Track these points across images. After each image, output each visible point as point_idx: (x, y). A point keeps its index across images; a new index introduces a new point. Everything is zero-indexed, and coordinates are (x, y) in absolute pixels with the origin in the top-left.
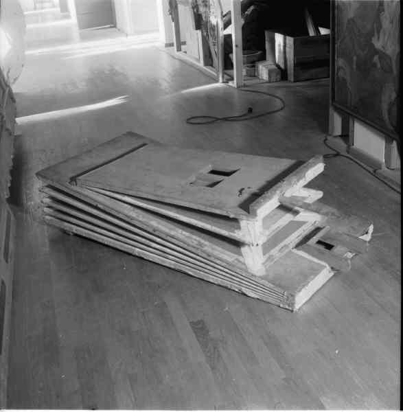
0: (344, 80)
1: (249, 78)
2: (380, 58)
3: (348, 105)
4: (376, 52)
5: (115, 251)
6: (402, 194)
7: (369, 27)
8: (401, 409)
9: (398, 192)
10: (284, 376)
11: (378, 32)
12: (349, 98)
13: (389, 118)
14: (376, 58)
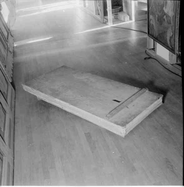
0: (153, 25)
1: (115, 20)
2: (166, 17)
3: (154, 36)
4: (165, 14)
5: (171, 73)
6: (183, 77)
7: (162, 3)
8: (183, 185)
9: (180, 76)
10: (120, 156)
11: (166, 5)
12: (155, 33)
13: (170, 44)
14: (165, 16)
